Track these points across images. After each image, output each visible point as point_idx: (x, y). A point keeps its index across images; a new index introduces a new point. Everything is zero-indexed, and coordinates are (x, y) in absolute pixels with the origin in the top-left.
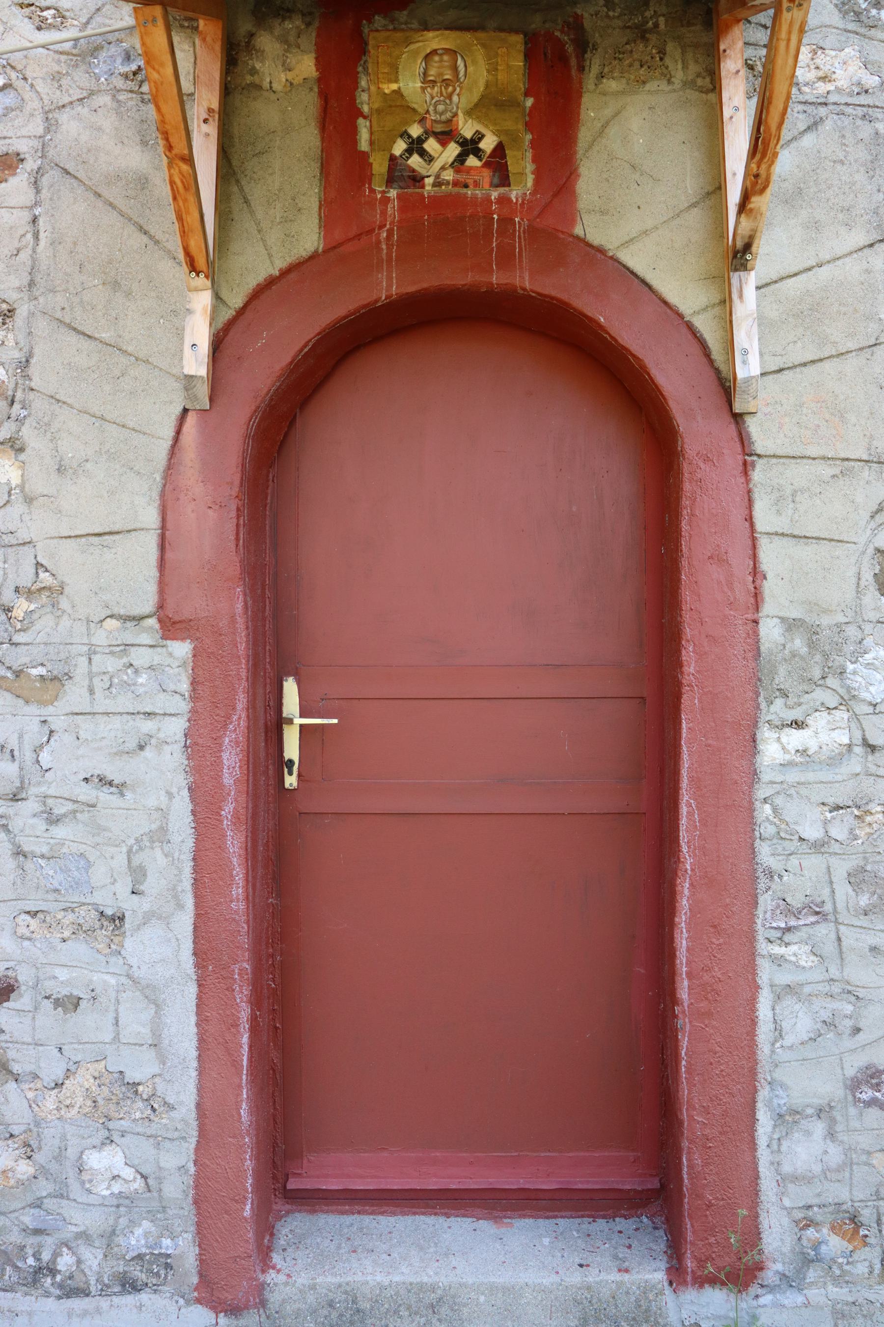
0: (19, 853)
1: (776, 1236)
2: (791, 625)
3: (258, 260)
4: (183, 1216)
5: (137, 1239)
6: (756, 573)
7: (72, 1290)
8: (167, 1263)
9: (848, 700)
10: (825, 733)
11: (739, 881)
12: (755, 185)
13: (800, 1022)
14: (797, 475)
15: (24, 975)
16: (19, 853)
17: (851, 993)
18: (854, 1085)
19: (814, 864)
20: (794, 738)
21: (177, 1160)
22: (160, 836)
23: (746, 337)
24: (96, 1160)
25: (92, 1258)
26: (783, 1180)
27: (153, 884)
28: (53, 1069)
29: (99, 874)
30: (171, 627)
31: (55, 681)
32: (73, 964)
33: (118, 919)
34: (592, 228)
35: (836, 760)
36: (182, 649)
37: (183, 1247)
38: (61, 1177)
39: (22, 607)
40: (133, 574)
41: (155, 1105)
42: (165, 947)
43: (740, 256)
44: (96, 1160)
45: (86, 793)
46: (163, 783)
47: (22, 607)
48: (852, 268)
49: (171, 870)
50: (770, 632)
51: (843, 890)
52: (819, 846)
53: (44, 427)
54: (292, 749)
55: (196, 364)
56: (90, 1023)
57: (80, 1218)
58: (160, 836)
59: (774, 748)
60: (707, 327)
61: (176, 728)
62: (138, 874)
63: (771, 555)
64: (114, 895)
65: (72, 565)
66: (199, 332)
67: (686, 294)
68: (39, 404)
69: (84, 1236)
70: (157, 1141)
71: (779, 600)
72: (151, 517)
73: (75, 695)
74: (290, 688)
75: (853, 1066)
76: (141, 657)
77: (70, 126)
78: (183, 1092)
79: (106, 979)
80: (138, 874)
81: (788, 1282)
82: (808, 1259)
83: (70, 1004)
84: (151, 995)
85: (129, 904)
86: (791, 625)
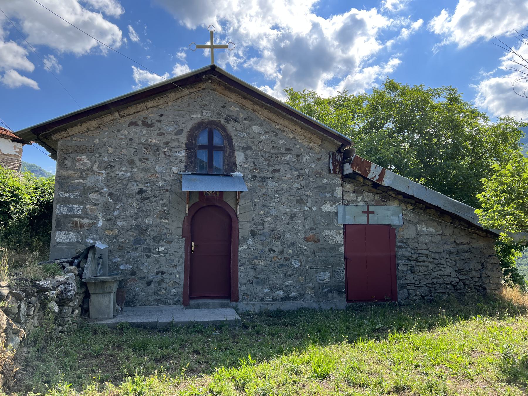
0: (166, 259)
1: (240, 296)
2: (242, 237)
3: (192, 202)
4: (181, 296)
5: (176, 299)
6: (239, 232)
7: (169, 304)
8: (179, 301)
9: (247, 244)
10: (245, 247)
11: (237, 261)
12: (238, 199)
13: (243, 275)
14: (243, 223)
15: (166, 271)
16: (166, 259)
17: (247, 272)
18: (248, 281)
19: (244, 260)
20: (242, 247)
21: (181, 290)
22: (181, 257)
23: (238, 211)
24: (173, 291)
25: (171, 301)
26: (241, 291)
27: (180, 262)
28: (168, 281)
29: (175, 261)
30: (183, 237)
31: (171, 242)
32: (171, 270)
33: (176, 265)
34: (224, 200)
35: (246, 249)
36: (184, 239)
37: (181, 299)
38: (169, 293)
39: (168, 235)
40: (180, 231)
41: (179, 284)
42: (181, 268)
43: (238, 203)
44: (173, 291)
45: (174, 253)
46: (182, 251)
47: (168, 235)
48: (249, 204)
49: (182, 260)
50: (240, 237)
51: (247, 262)
52: (244, 258)
53: (171, 217)
54: (193, 249)
55: (187, 212)
56: (173, 276)
57: (170, 297)
58: (181, 257)
59: (240, 248)
60: (235, 209)
61: (183, 246)
62: (179, 261)
63: (240, 230)
64: (176, 262)
65: (174, 231)
66: (187, 209)
67: (233, 206)
68: (170, 215)
69: (171, 299)
70: (179, 288)
71: (241, 235)
72: (182, 226)
73: (173, 243)
74: (193, 243)
75: (248, 279)
76: (180, 240)
77: (173, 187)
78: (182, 283)
79: (175, 272)
80: (179, 261)
81: (242, 301)
82: (243, 299)
83: (171, 274)
84: (179, 273)
85: (178, 264)
86: (242, 237)
